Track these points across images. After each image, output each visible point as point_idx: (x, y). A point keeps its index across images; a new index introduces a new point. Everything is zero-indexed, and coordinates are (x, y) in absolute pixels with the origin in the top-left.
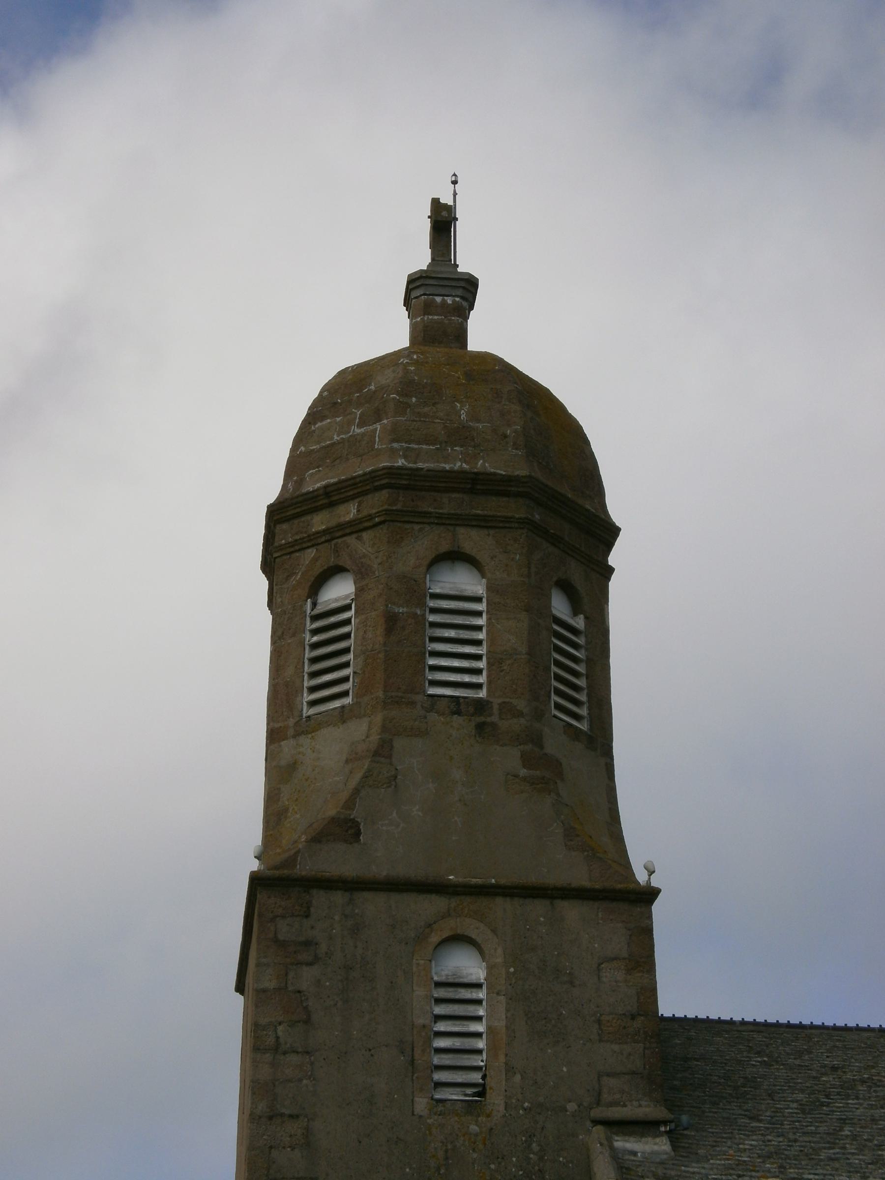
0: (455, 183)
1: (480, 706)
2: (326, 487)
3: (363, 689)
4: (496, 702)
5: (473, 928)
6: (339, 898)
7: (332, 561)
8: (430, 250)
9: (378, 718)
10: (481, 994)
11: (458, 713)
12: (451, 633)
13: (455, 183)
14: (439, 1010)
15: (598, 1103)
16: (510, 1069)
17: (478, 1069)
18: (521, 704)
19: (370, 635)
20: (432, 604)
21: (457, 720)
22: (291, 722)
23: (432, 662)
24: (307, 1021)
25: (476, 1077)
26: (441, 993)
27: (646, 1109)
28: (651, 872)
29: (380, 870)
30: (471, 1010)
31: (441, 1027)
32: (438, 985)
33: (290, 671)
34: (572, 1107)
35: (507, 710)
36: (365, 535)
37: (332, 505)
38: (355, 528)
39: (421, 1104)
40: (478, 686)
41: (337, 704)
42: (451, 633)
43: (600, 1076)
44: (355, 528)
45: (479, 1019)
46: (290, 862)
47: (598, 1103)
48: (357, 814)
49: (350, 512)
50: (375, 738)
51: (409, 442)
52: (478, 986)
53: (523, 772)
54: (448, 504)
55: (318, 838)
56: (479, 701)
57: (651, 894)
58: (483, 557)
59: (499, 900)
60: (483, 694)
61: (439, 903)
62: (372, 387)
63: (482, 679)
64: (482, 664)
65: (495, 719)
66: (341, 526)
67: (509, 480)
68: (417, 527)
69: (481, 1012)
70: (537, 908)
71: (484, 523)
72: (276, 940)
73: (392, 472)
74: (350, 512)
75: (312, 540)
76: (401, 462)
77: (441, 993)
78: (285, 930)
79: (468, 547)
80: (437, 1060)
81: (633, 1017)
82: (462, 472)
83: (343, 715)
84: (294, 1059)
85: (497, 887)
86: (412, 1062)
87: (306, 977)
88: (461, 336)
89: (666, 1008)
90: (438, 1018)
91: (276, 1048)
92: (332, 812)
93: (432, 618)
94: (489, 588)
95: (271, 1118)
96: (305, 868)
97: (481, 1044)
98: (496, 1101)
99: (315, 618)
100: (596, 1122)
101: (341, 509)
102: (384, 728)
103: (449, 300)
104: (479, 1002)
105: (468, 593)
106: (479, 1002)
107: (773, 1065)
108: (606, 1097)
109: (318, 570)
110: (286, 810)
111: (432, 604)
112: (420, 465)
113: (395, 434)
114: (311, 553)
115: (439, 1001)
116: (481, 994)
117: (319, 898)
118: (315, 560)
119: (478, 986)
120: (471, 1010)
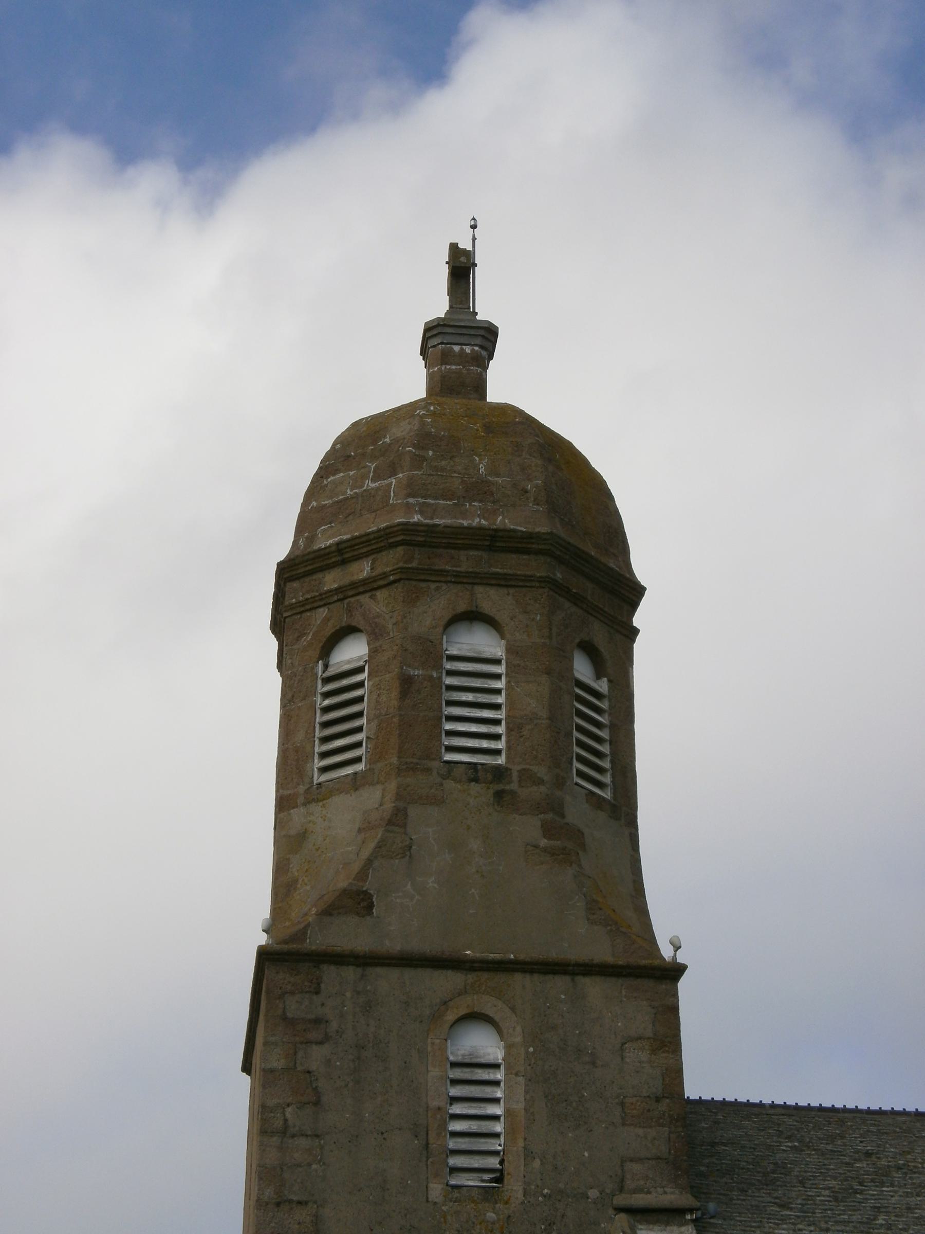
1: (499, 773)
2: (338, 544)
3: (377, 755)
4: (515, 769)
5: (490, 1005)
6: (350, 973)
7: (345, 621)
9: (392, 786)
10: (499, 1075)
11: (476, 780)
12: (469, 697)
13: (474, 227)
14: (455, 1091)
15: (621, 1190)
16: (528, 1154)
18: (541, 771)
19: (384, 698)
21: (475, 788)
22: (301, 789)
23: (449, 726)
25: (493, 1162)
27: (671, 1197)
29: (394, 946)
30: (488, 1092)
31: (457, 1109)
32: (454, 1065)
33: (300, 736)
34: (593, 1193)
35: (527, 777)
36: (378, 594)
38: (369, 586)
39: (436, 1190)
41: (349, 770)
42: (469, 697)
43: (623, 1161)
44: (369, 586)
45: (496, 1101)
46: (300, 936)
47: (621, 1190)
48: (370, 885)
49: (363, 570)
50: (389, 806)
52: (496, 1066)
53: (544, 842)
54: (466, 561)
55: (329, 911)
56: (498, 768)
59: (518, 976)
60: (501, 760)
64: (501, 729)
65: (514, 786)
66: (354, 585)
67: (530, 537)
69: (499, 1094)
70: (558, 985)
71: (504, 581)
72: (284, 1018)
73: (407, 529)
74: (363, 570)
76: (416, 518)
78: (294, 1007)
80: (452, 1144)
81: (658, 1100)
82: (481, 528)
83: (356, 782)
84: (303, 1142)
87: (316, 1057)
88: (480, 388)
89: (694, 1089)
90: (454, 1100)
91: (284, 1131)
92: (343, 884)
93: (449, 681)
94: (509, 650)
96: (316, 942)
97: (498, 1128)
98: (514, 1187)
99: (327, 680)
100: (619, 1210)
102: (399, 796)
103: (468, 349)
106: (496, 1083)
107: (804, 1151)
109: (329, 631)
110: (295, 881)
112: (437, 521)
113: (411, 488)
114: (323, 612)
115: (455, 1082)
117: (330, 973)
118: (326, 620)
119: (496, 1066)
120: (488, 1092)
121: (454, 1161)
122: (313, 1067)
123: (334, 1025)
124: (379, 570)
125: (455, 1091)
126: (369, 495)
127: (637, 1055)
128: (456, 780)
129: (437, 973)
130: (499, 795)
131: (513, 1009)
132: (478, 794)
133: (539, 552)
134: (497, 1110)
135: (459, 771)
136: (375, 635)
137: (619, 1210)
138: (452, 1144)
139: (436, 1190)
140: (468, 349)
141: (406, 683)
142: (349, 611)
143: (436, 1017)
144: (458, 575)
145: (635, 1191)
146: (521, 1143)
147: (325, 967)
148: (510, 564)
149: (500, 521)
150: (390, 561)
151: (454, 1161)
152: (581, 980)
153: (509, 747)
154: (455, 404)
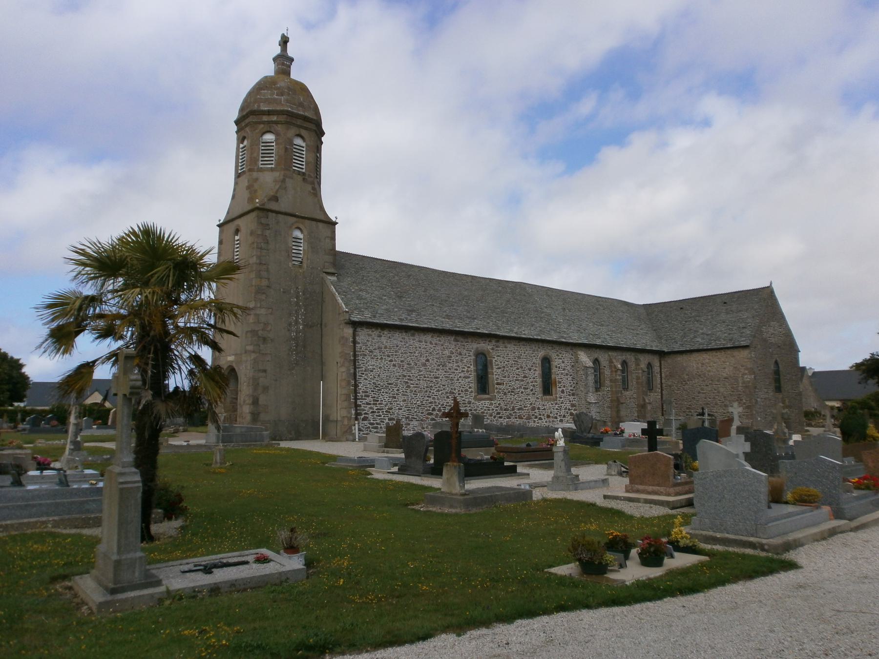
0: (287, 30)
1: (304, 174)
2: (269, 110)
3: (277, 164)
4: (307, 173)
5: (301, 226)
6: (274, 214)
7: (268, 129)
8: (280, 47)
9: (282, 173)
10: (302, 241)
11: (299, 174)
12: (298, 155)
13: (287, 30)
14: (294, 244)
15: (324, 268)
16: (308, 259)
17: (301, 258)
18: (312, 175)
19: (280, 151)
20: (294, 146)
21: (299, 176)
22: (256, 168)
23: (294, 161)
24: (268, 243)
25: (300, 260)
26: (294, 240)
27: (332, 270)
28: (336, 219)
29: (283, 210)
30: (299, 244)
31: (294, 247)
32: (293, 238)
33: (255, 155)
34: (319, 268)
35: (310, 176)
36: (278, 125)
37: (269, 115)
38: (276, 123)
39: (290, 264)
40: (302, 169)
41: (270, 166)
42: (298, 155)
43: (325, 262)
44: (276, 123)
45: (301, 247)
46: (263, 204)
47: (324, 268)
48: (278, 195)
49: (275, 118)
50: (282, 177)
51: (291, 104)
52: (301, 239)
53: (312, 191)
54: (299, 122)
55: (270, 200)
56: (303, 172)
57: (336, 223)
58: (305, 137)
59: (306, 220)
60: (304, 171)
61: (293, 219)
62: (278, 86)
63: (304, 167)
64: (304, 163)
65: (307, 177)
66: (272, 121)
67: (312, 119)
68: (292, 126)
69: (302, 245)
70: (314, 223)
71: (306, 129)
72: (261, 223)
73: (288, 111)
74: (275, 118)
75: (263, 123)
76: (290, 109)
77: (294, 240)
78: (263, 221)
79: (303, 134)
80: (293, 255)
81: (331, 250)
82: (303, 115)
83: (272, 170)
84: (265, 251)
85: (307, 217)
86: (289, 255)
87: (267, 233)
88: (289, 74)
89: (337, 249)
90: (294, 245)
91: (261, 248)
92: (272, 194)
93: (294, 150)
94: (306, 145)
95: (260, 264)
96: (267, 206)
97: (302, 252)
98: (305, 265)
99: (263, 143)
100: (324, 272)
101: (271, 116)
102: (284, 176)
103: (288, 63)
104: (301, 243)
105: (302, 145)
106: (301, 243)
107: (733, 305)
108: (326, 267)
109: (264, 131)
110: (257, 190)
111: (294, 146)
112: (294, 111)
113: (287, 101)
114: (262, 126)
115: (294, 242)
116: (302, 241)
117: (270, 214)
118: (263, 128)
119: (301, 239)
120: (299, 244)
121: (294, 259)
122: (267, 235)
123: (271, 226)
124: (278, 120)
125: (294, 244)
126: (275, 100)
127: (328, 240)
128: (295, 174)
129: (292, 218)
130: (304, 179)
131: (305, 228)
132: (300, 178)
133: (314, 124)
134: (301, 249)
135: (296, 172)
136: (277, 134)
137: (324, 272)
138: (293, 255)
139: (290, 264)
140: (288, 63)
141: (286, 149)
142: (270, 127)
143: (291, 227)
144: (297, 125)
145: (326, 269)
146: (306, 256)
147: (269, 213)
148: (306, 124)
149: (307, 114)
150: (282, 118)
151: (294, 259)
152: (319, 223)
153: (305, 167)
154: (282, 76)
